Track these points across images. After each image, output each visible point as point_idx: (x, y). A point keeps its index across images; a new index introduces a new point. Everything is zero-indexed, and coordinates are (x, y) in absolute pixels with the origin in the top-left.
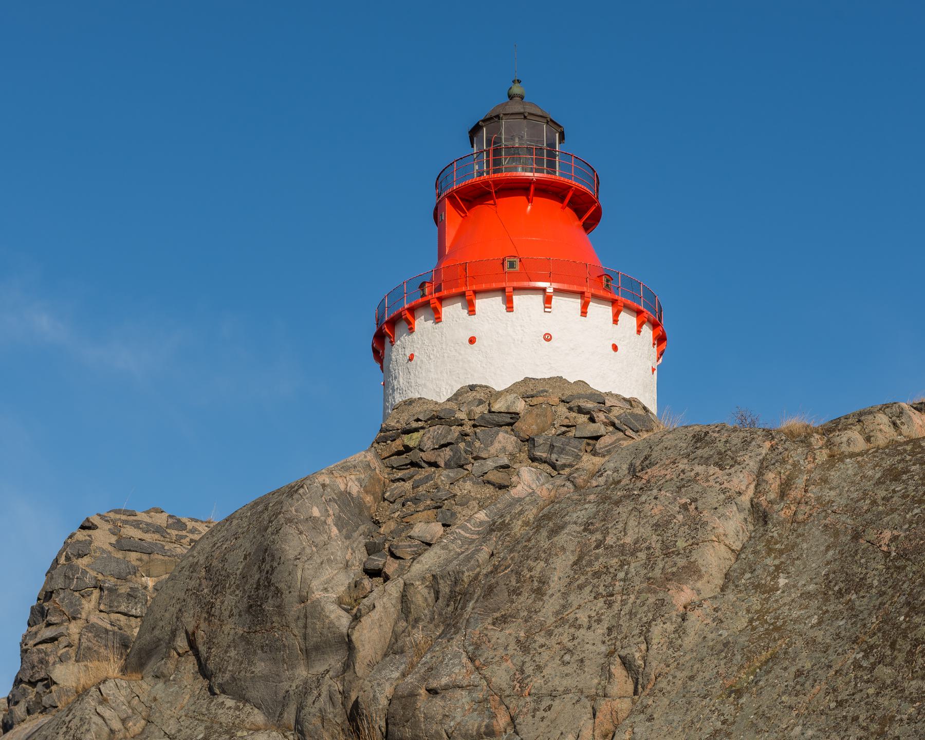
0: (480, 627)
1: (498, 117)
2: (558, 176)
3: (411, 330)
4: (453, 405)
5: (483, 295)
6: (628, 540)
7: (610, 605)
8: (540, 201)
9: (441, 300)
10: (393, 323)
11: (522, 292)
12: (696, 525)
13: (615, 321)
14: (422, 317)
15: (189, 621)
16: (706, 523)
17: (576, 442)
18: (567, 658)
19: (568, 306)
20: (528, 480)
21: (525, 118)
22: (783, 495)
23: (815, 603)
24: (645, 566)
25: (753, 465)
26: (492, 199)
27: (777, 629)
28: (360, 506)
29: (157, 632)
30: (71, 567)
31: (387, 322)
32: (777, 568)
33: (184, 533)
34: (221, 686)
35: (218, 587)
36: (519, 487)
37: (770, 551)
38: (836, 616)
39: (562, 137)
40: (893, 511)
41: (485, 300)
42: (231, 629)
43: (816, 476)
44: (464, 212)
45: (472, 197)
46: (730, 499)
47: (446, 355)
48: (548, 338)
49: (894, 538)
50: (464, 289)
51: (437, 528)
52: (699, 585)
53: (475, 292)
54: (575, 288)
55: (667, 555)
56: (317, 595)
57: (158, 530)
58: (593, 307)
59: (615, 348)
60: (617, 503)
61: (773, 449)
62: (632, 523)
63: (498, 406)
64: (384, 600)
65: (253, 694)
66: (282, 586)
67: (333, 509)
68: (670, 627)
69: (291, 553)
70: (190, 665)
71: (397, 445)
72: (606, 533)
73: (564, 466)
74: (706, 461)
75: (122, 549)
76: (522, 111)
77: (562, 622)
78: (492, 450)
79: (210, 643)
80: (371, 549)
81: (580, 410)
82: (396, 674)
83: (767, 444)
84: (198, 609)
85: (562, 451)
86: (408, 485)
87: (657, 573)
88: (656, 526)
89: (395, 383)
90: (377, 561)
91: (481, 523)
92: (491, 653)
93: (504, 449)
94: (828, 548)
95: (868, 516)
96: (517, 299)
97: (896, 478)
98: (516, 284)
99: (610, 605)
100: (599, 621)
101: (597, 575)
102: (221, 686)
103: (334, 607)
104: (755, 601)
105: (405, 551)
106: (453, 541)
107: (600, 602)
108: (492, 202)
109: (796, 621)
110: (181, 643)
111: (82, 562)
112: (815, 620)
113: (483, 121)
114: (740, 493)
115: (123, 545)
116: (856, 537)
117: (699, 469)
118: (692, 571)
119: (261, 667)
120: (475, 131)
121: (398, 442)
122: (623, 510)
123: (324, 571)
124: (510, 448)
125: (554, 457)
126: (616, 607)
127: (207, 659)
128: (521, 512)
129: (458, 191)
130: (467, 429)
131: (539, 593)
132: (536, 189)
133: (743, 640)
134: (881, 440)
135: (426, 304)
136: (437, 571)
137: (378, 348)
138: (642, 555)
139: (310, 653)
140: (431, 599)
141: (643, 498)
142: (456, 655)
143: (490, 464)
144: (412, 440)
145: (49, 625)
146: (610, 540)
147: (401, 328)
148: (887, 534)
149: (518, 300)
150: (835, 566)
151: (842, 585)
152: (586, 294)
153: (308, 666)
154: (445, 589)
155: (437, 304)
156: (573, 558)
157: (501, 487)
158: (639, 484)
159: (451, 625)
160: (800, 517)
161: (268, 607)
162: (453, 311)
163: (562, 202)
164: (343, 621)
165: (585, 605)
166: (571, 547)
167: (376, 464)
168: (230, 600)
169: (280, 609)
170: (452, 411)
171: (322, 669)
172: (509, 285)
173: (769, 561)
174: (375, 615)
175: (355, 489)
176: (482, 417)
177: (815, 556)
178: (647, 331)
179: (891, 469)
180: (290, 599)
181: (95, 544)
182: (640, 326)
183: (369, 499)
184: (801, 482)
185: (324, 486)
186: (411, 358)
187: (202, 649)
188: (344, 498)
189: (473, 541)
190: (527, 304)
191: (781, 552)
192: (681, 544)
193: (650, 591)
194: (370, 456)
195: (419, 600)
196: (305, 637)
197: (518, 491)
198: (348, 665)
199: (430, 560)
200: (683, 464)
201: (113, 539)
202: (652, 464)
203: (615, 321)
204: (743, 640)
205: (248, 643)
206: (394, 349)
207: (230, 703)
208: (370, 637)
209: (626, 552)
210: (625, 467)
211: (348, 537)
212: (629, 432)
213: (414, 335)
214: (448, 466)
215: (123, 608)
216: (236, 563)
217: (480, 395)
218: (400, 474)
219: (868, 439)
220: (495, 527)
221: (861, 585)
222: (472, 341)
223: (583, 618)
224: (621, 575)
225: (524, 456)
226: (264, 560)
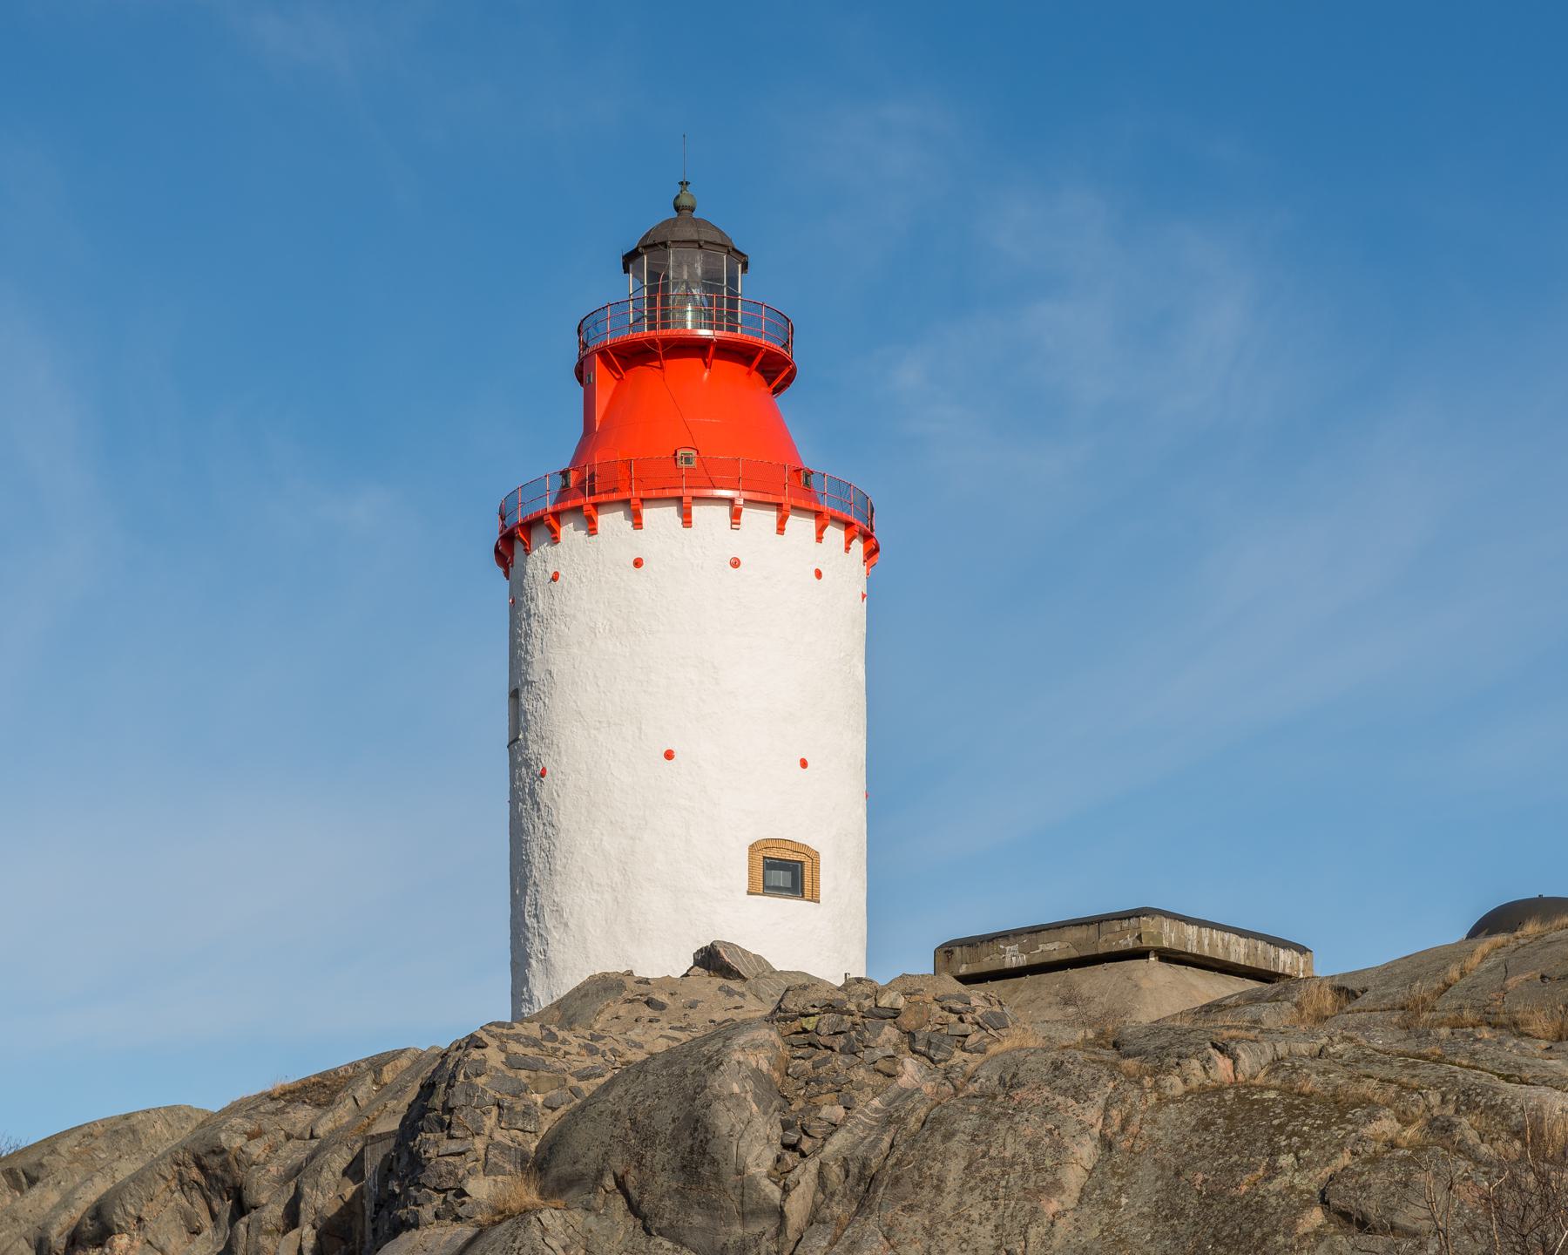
0: (892, 1212)
1: (664, 244)
2: (740, 334)
4: (841, 995)
6: (1007, 1154)
7: (996, 1207)
8: (722, 366)
9: (596, 506)
12: (1059, 1148)
13: (819, 539)
15: (618, 1163)
16: (1066, 1148)
17: (948, 1040)
18: (964, 1246)
19: (760, 520)
20: (911, 1071)
22: (1123, 1129)
23: (1148, 1223)
24: (1021, 1177)
25: (1101, 1102)
27: (1121, 1241)
28: (770, 1081)
29: (579, 1167)
30: (471, 1085)
32: (1120, 1188)
33: (557, 1045)
34: (658, 1229)
35: (648, 1139)
36: (904, 1078)
37: (1114, 1174)
38: (1164, 1236)
39: (745, 267)
40: (1204, 1157)
42: (664, 1181)
43: (1148, 1116)
46: (1084, 1131)
48: (736, 563)
49: (1205, 1181)
51: (840, 1111)
52: (1063, 1198)
54: (770, 498)
55: (1038, 1170)
56: (753, 1170)
57: (536, 1043)
58: (794, 522)
59: (819, 574)
60: (996, 1119)
61: (1115, 1088)
62: (1010, 1140)
63: (883, 1002)
64: (805, 1175)
65: (690, 1240)
66: (718, 1157)
67: (749, 1085)
68: (1042, 1230)
69: (725, 1130)
70: (620, 1203)
71: (795, 1026)
72: (989, 1146)
73: (940, 1061)
74: (1065, 1092)
75: (512, 1067)
76: (695, 237)
77: (959, 1216)
78: (880, 1041)
79: (642, 1188)
80: (786, 1126)
81: (951, 1010)
82: (824, 1244)
83: (1111, 1085)
84: (626, 1156)
85: (938, 1048)
86: (808, 1064)
87: (1031, 1185)
88: (1029, 1145)
89: (532, 606)
90: (793, 1137)
91: (876, 1110)
92: (903, 1236)
93: (889, 1040)
94: (1157, 1179)
95: (1187, 1158)
96: (697, 511)
97: (1206, 1129)
98: (695, 492)
99: (996, 1207)
100: (988, 1219)
101: (984, 1180)
102: (658, 1229)
103: (767, 1182)
104: (1105, 1216)
105: (817, 1130)
106: (856, 1125)
107: (988, 1204)
108: (657, 364)
109: (1135, 1236)
110: (609, 1182)
111: (481, 1081)
112: (1148, 1237)
114: (1092, 1126)
115: (513, 1063)
116: (1178, 1174)
117: (1060, 1099)
118: (1057, 1187)
119: (698, 1220)
120: (630, 259)
121: (797, 1023)
122: (1002, 1126)
123: (754, 1146)
124: (894, 1040)
125: (932, 1052)
126: (1001, 1208)
127: (640, 1202)
128: (913, 1110)
130: (858, 1020)
131: (938, 1189)
133: (1097, 1247)
134: (1194, 1083)
136: (847, 1153)
138: (1019, 1168)
139: (744, 1217)
140: (842, 1177)
141: (1017, 1119)
142: (873, 1233)
143: (878, 1053)
144: (810, 1024)
145: (450, 1137)
146: (993, 1152)
148: (1200, 1177)
150: (1162, 1195)
151: (1167, 1212)
153: (744, 1226)
154: (854, 1169)
156: (964, 1164)
157: (889, 1076)
158: (1013, 1104)
159: (864, 1205)
160: (1137, 1149)
161: (705, 1171)
162: (612, 521)
164: (775, 1193)
165: (976, 1206)
166: (962, 1153)
167: (779, 1042)
168: (659, 1156)
169: (717, 1176)
170: (843, 1002)
171: (757, 1230)
172: (686, 493)
173: (1113, 1182)
174: (800, 1189)
175: (764, 1066)
176: (870, 1011)
177: (1146, 1186)
178: (858, 546)
179: (1202, 1120)
180: (728, 1170)
181: (490, 1063)
182: (849, 542)
183: (776, 1075)
184: (1137, 1119)
185: (739, 1063)
186: (555, 578)
187: (634, 1193)
188: (757, 1074)
189: (872, 1128)
191: (1123, 1176)
192: (1048, 1163)
193: (1026, 1199)
194: (774, 1036)
195: (833, 1177)
196: (742, 1203)
197: (905, 1081)
198: (781, 1229)
199: (838, 1141)
200: (1046, 1092)
201: (503, 1057)
202: (1021, 1085)
203: (819, 539)
204: (1097, 1247)
205: (683, 1196)
207: (667, 1244)
208: (797, 1208)
209: (1007, 1165)
210: (996, 1077)
211: (765, 1113)
212: (991, 1031)
214: (842, 1051)
215: (520, 1125)
216: (665, 1119)
217: (868, 990)
218: (799, 1053)
219: (1185, 1081)
220: (890, 1119)
221: (1180, 1213)
222: (638, 563)
223: (975, 1215)
224: (1003, 1183)
225: (905, 1047)
226: (696, 1129)
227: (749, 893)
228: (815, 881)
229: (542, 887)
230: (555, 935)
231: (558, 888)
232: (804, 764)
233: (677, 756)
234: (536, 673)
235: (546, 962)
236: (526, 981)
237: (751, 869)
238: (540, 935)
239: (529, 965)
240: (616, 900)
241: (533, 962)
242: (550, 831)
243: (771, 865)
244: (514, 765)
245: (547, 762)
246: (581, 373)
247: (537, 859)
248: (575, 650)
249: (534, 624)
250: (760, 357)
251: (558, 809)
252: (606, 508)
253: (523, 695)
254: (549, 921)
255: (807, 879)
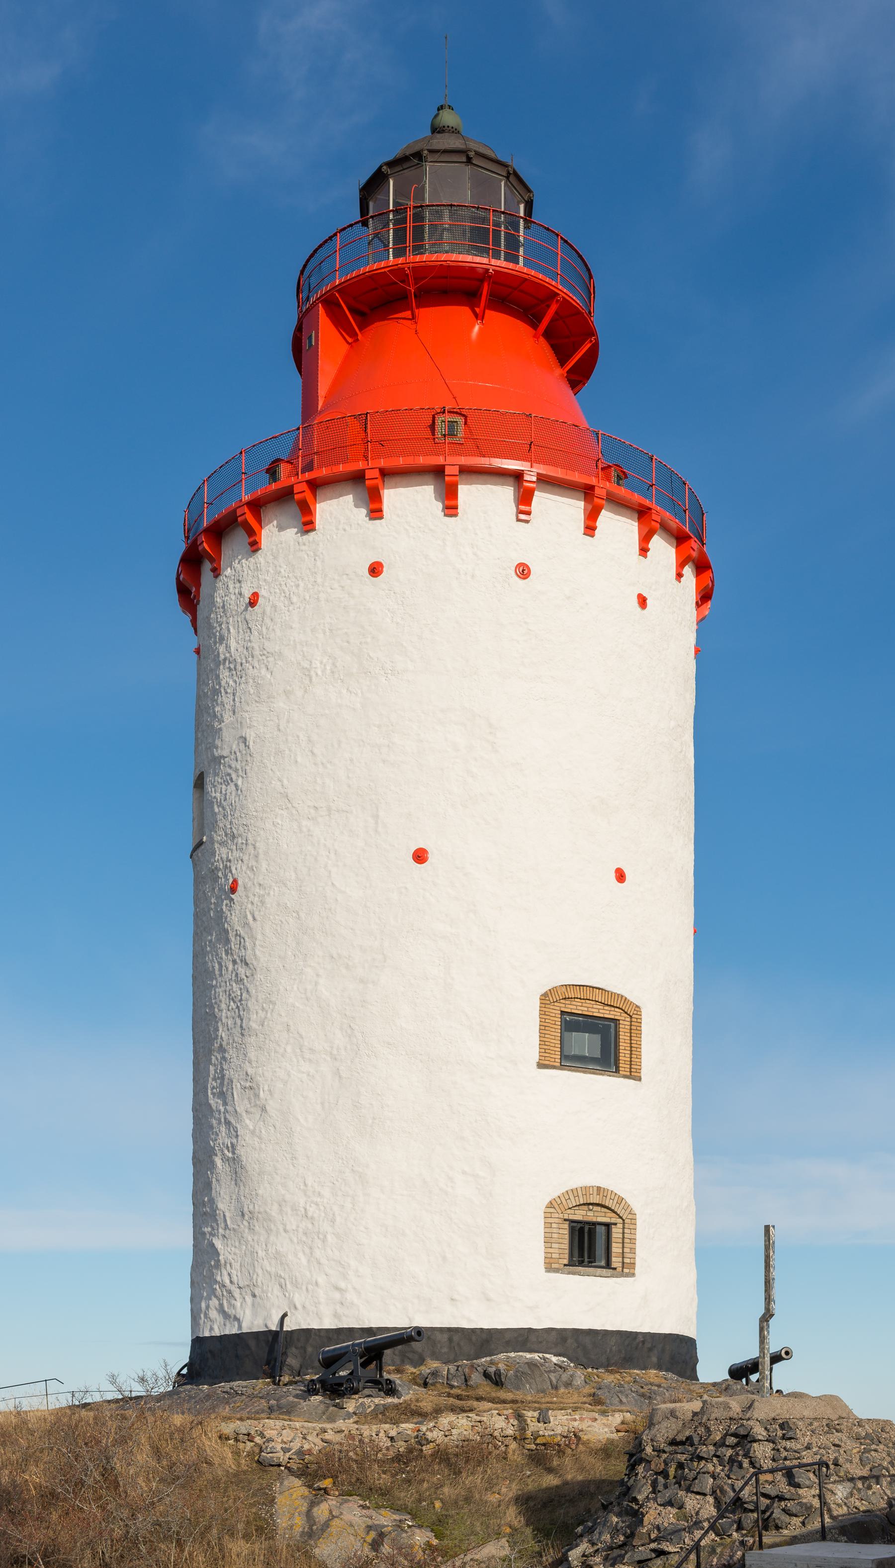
1: (418, 155)
3: (255, 546)
5: (397, 479)
9: (315, 486)
10: (219, 531)
11: (474, 477)
14: (275, 523)
19: (560, 511)
21: (469, 160)
26: (408, 307)
31: (207, 531)
41: (402, 490)
44: (354, 335)
45: (369, 303)
47: (322, 596)
50: (361, 465)
53: (385, 473)
58: (607, 519)
59: (642, 601)
89: (222, 649)
96: (467, 492)
98: (464, 461)
108: (408, 314)
113: (390, 164)
129: (343, 289)
132: (492, 294)
135: (284, 496)
137: (188, 583)
147: (237, 541)
149: (469, 493)
152: (597, 491)
155: (308, 495)
162: (337, 511)
163: (534, 326)
172: (453, 462)
182: (681, 565)
186: (253, 601)
190: (486, 502)
206: (219, 584)
213: (260, 557)
222: (375, 570)
227: (541, 1066)
228: (634, 1049)
229: (231, 1053)
230: (248, 1123)
231: (252, 1055)
232: (621, 876)
233: (432, 858)
234: (227, 744)
235: (235, 1162)
236: (208, 1185)
237: (543, 1028)
238: (228, 1123)
239: (213, 1163)
240: (337, 1073)
241: (218, 1161)
242: (242, 971)
243: (573, 1023)
244: (198, 881)
245: (240, 872)
246: (301, 351)
247: (225, 1014)
248: (281, 704)
249: (224, 674)
250: (554, 307)
251: (253, 938)
252: (328, 491)
253: (208, 779)
254: (241, 1103)
255: (623, 1045)
